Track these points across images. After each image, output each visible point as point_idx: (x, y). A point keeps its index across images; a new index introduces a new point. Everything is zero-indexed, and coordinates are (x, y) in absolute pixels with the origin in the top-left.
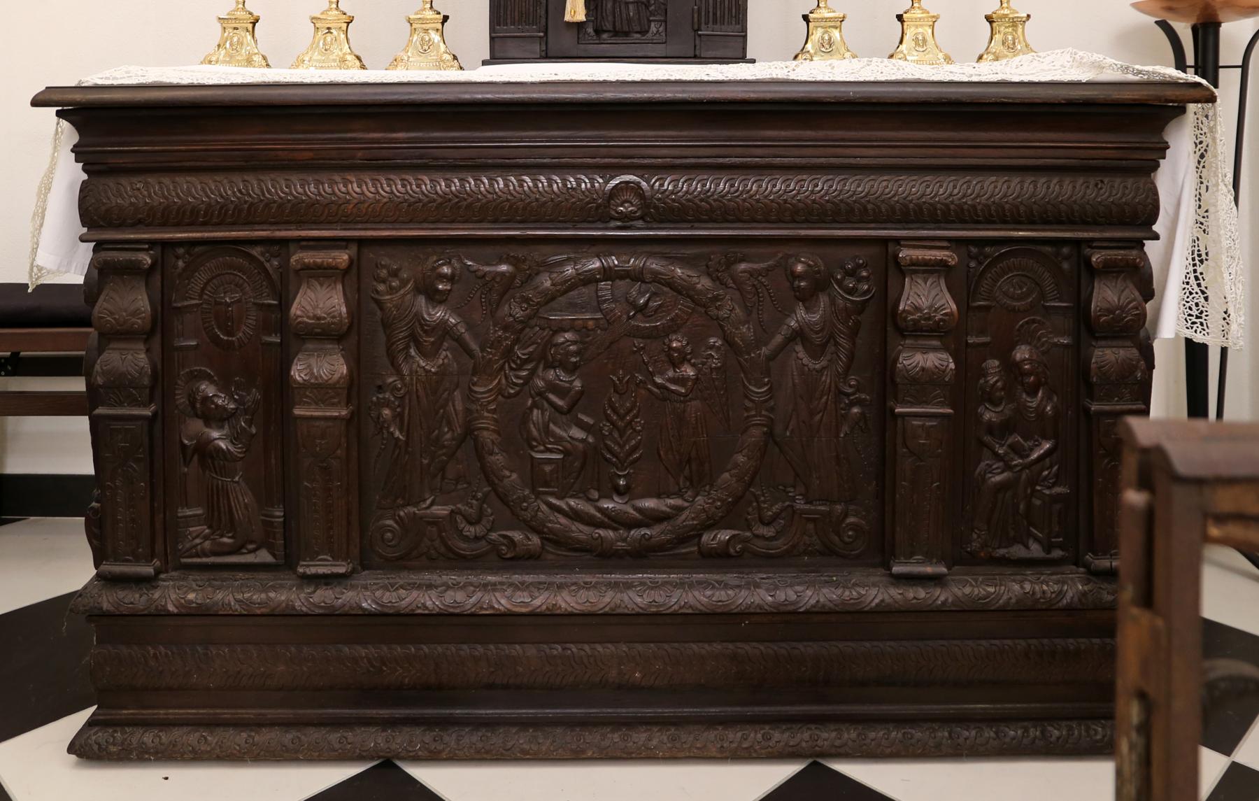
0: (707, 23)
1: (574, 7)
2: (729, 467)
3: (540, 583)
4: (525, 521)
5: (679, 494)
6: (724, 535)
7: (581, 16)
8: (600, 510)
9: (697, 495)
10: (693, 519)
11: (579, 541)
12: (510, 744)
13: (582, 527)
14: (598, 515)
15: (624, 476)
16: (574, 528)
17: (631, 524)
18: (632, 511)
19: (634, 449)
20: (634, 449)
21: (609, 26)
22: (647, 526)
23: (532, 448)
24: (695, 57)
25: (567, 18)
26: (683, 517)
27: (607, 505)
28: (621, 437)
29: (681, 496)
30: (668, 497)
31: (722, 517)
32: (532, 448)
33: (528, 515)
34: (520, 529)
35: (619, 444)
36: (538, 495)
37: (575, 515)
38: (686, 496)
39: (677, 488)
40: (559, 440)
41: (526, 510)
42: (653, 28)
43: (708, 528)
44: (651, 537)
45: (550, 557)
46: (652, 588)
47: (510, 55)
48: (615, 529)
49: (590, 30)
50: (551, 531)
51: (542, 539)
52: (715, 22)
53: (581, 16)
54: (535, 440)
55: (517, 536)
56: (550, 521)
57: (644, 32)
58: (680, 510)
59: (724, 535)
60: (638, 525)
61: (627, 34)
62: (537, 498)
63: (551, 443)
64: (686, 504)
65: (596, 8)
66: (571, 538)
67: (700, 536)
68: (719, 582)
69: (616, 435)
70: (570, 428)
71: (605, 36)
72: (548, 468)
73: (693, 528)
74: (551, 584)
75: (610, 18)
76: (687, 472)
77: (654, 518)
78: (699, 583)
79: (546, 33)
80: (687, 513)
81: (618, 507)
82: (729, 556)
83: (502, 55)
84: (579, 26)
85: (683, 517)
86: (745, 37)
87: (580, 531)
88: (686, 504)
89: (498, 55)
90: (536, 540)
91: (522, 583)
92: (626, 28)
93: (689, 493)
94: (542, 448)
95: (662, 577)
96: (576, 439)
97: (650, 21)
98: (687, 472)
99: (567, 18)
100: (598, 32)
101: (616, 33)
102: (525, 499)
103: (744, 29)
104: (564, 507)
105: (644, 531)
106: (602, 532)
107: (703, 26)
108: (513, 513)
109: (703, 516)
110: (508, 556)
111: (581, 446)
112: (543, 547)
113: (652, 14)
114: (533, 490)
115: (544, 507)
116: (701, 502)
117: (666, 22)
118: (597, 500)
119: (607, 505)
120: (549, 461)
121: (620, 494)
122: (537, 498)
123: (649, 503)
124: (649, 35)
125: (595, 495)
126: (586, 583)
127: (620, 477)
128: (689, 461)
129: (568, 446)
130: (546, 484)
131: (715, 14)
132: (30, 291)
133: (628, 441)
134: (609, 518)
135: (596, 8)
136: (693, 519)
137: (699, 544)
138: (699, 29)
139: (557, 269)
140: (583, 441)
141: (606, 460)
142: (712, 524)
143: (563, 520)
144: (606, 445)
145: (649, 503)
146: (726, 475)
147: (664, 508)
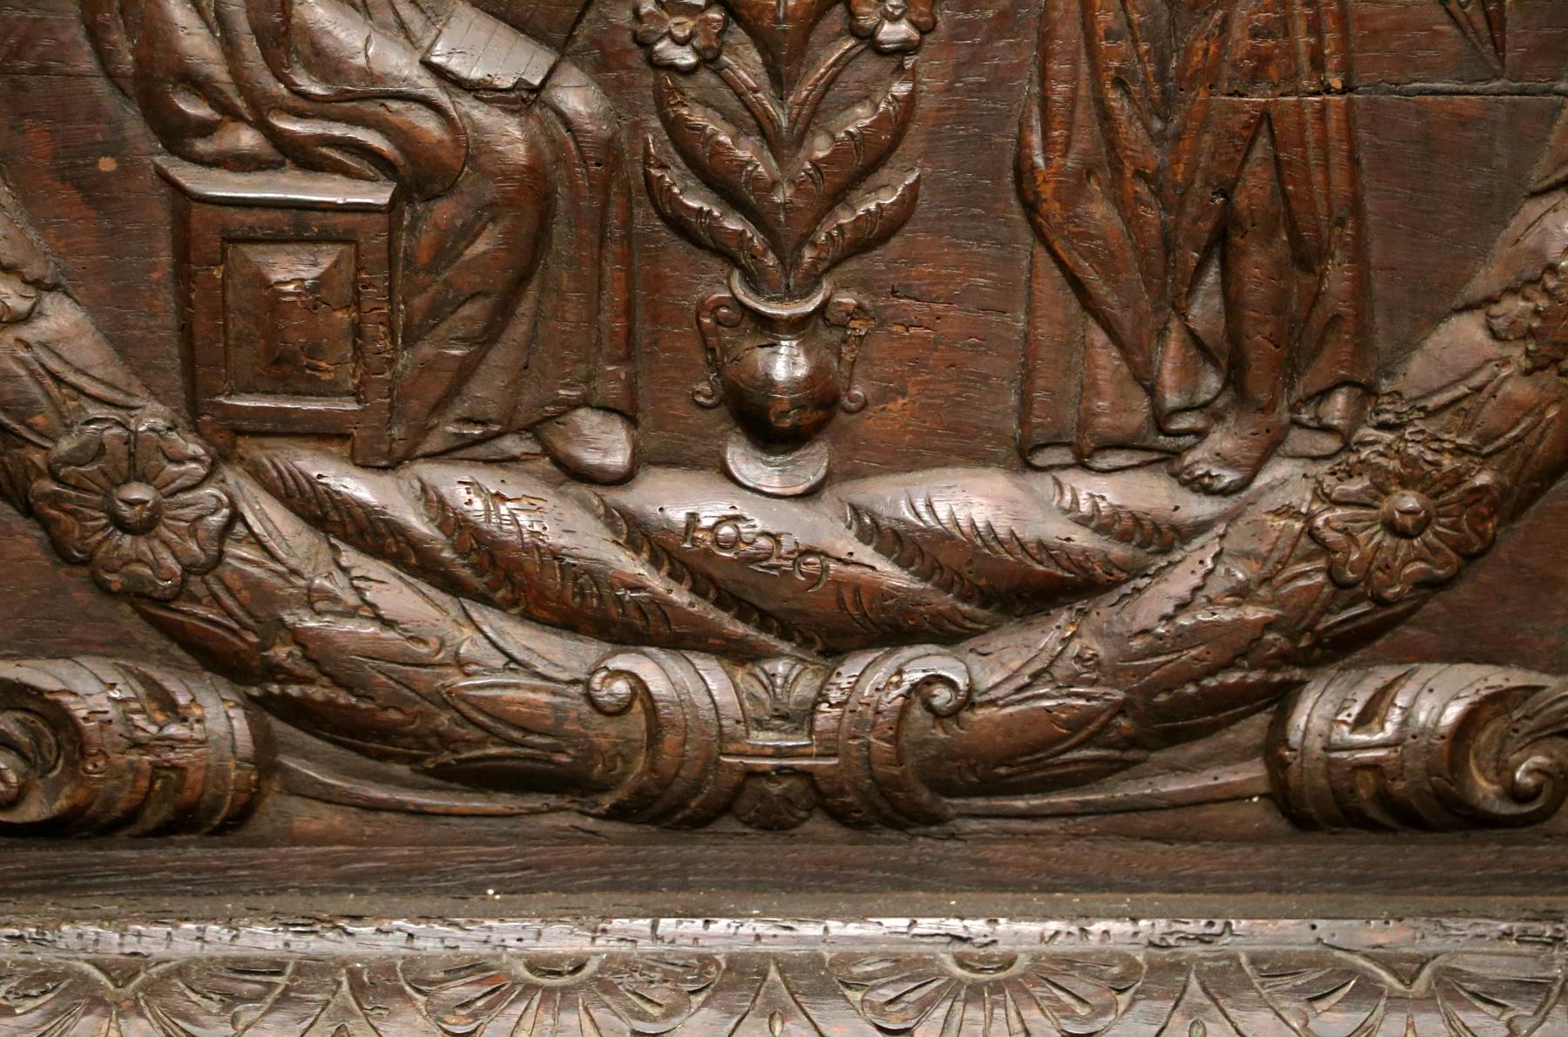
2: (1484, 280)
3: (243, 968)
4: (139, 596)
5: (1157, 446)
6: (1437, 699)
8: (638, 533)
9: (1271, 448)
10: (1242, 594)
11: (499, 720)
13: (520, 637)
14: (630, 565)
15: (796, 326)
16: (469, 645)
17: (842, 624)
18: (844, 542)
19: (867, 160)
20: (867, 160)
22: (947, 634)
23: (177, 136)
26: (1180, 583)
27: (679, 501)
28: (780, 81)
29: (1167, 460)
30: (1082, 463)
31: (1429, 586)
32: (177, 136)
33: (160, 559)
34: (114, 647)
35: (764, 130)
36: (229, 440)
37: (491, 573)
38: (1199, 459)
39: (1138, 413)
40: (361, 95)
41: (145, 527)
43: (1337, 648)
44: (969, 701)
45: (311, 818)
46: (975, 993)
48: (736, 654)
50: (320, 657)
51: (258, 706)
54: (199, 85)
55: (91, 689)
56: (311, 599)
58: (1159, 538)
59: (1437, 699)
60: (892, 627)
62: (220, 458)
63: (307, 106)
64: (1198, 508)
66: (447, 699)
67: (1283, 698)
68: (1407, 966)
69: (746, 64)
70: (890, 85)
72: (291, 270)
73: (1241, 646)
74: (314, 969)
76: (1205, 310)
77: (1016, 587)
78: (1275, 967)
80: (1201, 552)
81: (759, 520)
82: (1475, 821)
85: (1180, 583)
87: (517, 664)
88: (1198, 508)
90: (218, 718)
91: (124, 970)
93: (1221, 440)
94: (247, 139)
95: (1022, 933)
96: (479, 90)
98: (1205, 310)
102: (136, 460)
104: (418, 523)
105: (919, 663)
106: (657, 672)
108: (59, 550)
109: (1310, 577)
110: (34, 810)
111: (510, 136)
112: (264, 742)
114: (194, 409)
115: (268, 516)
116: (1302, 497)
118: (623, 479)
119: (679, 501)
120: (298, 225)
121: (771, 438)
122: (220, 458)
123: (968, 501)
125: (609, 446)
126: (543, 966)
127: (769, 328)
128: (1222, 242)
129: (428, 125)
130: (286, 370)
132: (1312, 40)
133: (813, 117)
134: (702, 583)
136: (1242, 594)
137: (1273, 747)
140: (525, 99)
141: (681, 224)
142: (1353, 626)
143: (397, 595)
144: (676, 130)
145: (968, 501)
146: (1465, 334)
147: (1055, 529)
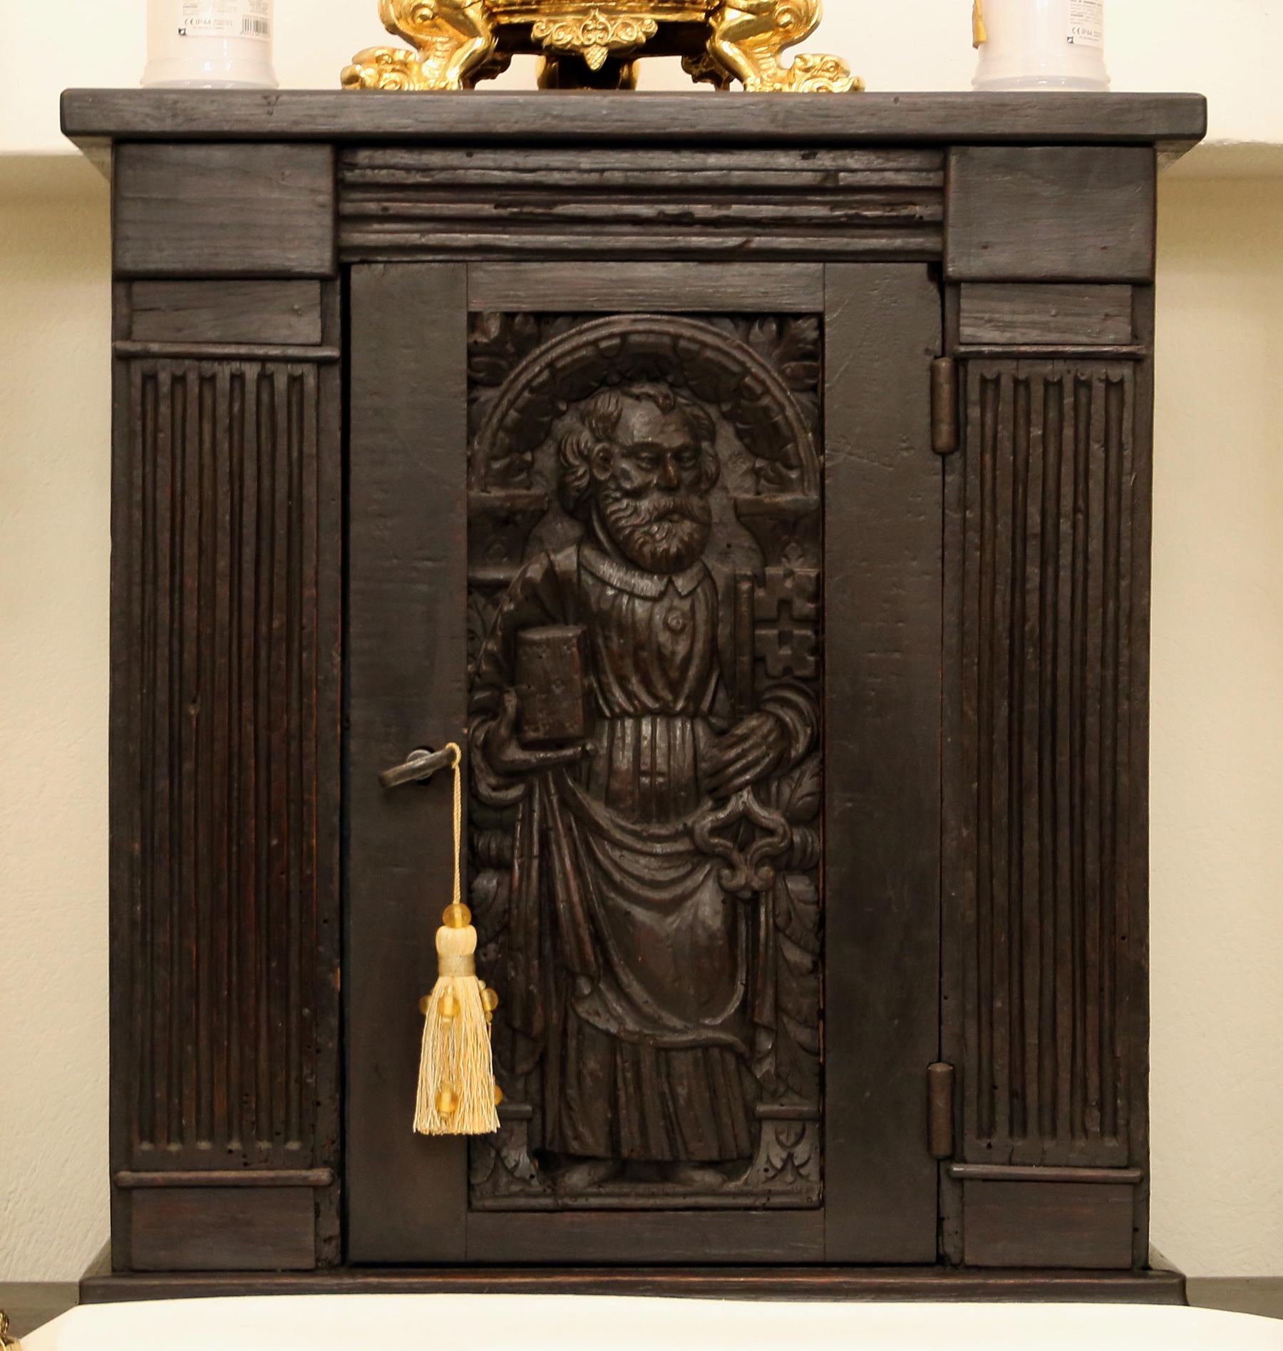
0: (987, 1130)
1: (450, 1080)
7: (480, 1116)
12: (766, 871)
21: (592, 1140)
24: (941, 1263)
25: (426, 1121)
42: (771, 1153)
47: (194, 1257)
49: (519, 1157)
52: (1018, 1125)
53: (480, 1116)
57: (731, 1163)
61: (665, 1171)
65: (542, 1063)
71: (577, 1178)
75: (600, 1110)
79: (340, 1170)
83: (165, 1257)
84: (472, 1144)
86: (1140, 1188)
89: (141, 1257)
92: (659, 1149)
97: (756, 1121)
99: (426, 1121)
100: (550, 1160)
101: (622, 1169)
103: (1137, 1156)
107: (972, 1142)
113: (763, 1090)
117: (820, 1118)
124: (754, 1175)
131: (1017, 1095)
135: (542, 1063)
138: (956, 1155)
139: (689, 903)
